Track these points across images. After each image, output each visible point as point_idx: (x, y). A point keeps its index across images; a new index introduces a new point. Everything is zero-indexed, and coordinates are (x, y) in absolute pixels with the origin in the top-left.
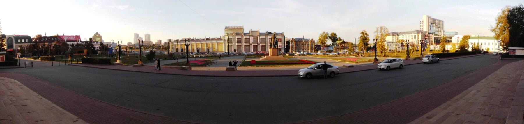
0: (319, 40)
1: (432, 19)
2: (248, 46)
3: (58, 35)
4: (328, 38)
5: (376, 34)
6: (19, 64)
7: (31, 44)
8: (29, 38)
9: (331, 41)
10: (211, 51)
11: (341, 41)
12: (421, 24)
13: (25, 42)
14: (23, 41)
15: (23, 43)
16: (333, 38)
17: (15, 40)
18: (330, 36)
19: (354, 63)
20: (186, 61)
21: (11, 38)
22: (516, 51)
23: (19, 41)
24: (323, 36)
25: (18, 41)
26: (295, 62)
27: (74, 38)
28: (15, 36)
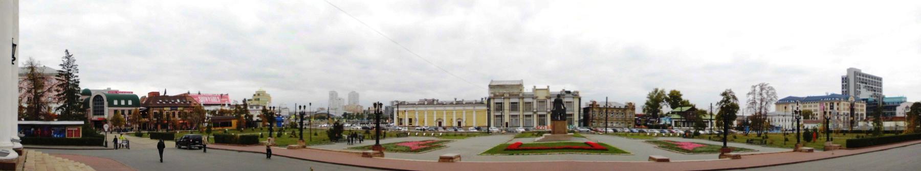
0: (646, 105)
1: (863, 75)
2: (530, 116)
3: (189, 93)
4: (664, 100)
5: (751, 97)
6: (106, 143)
7: (136, 110)
8: (134, 98)
9: (669, 106)
11: (690, 108)
12: (845, 84)
13: (126, 105)
14: (123, 103)
16: (673, 101)
17: (107, 101)
18: (668, 96)
21: (101, 97)
23: (116, 103)
24: (655, 96)
25: (113, 103)
26: (544, 147)
27: (218, 100)
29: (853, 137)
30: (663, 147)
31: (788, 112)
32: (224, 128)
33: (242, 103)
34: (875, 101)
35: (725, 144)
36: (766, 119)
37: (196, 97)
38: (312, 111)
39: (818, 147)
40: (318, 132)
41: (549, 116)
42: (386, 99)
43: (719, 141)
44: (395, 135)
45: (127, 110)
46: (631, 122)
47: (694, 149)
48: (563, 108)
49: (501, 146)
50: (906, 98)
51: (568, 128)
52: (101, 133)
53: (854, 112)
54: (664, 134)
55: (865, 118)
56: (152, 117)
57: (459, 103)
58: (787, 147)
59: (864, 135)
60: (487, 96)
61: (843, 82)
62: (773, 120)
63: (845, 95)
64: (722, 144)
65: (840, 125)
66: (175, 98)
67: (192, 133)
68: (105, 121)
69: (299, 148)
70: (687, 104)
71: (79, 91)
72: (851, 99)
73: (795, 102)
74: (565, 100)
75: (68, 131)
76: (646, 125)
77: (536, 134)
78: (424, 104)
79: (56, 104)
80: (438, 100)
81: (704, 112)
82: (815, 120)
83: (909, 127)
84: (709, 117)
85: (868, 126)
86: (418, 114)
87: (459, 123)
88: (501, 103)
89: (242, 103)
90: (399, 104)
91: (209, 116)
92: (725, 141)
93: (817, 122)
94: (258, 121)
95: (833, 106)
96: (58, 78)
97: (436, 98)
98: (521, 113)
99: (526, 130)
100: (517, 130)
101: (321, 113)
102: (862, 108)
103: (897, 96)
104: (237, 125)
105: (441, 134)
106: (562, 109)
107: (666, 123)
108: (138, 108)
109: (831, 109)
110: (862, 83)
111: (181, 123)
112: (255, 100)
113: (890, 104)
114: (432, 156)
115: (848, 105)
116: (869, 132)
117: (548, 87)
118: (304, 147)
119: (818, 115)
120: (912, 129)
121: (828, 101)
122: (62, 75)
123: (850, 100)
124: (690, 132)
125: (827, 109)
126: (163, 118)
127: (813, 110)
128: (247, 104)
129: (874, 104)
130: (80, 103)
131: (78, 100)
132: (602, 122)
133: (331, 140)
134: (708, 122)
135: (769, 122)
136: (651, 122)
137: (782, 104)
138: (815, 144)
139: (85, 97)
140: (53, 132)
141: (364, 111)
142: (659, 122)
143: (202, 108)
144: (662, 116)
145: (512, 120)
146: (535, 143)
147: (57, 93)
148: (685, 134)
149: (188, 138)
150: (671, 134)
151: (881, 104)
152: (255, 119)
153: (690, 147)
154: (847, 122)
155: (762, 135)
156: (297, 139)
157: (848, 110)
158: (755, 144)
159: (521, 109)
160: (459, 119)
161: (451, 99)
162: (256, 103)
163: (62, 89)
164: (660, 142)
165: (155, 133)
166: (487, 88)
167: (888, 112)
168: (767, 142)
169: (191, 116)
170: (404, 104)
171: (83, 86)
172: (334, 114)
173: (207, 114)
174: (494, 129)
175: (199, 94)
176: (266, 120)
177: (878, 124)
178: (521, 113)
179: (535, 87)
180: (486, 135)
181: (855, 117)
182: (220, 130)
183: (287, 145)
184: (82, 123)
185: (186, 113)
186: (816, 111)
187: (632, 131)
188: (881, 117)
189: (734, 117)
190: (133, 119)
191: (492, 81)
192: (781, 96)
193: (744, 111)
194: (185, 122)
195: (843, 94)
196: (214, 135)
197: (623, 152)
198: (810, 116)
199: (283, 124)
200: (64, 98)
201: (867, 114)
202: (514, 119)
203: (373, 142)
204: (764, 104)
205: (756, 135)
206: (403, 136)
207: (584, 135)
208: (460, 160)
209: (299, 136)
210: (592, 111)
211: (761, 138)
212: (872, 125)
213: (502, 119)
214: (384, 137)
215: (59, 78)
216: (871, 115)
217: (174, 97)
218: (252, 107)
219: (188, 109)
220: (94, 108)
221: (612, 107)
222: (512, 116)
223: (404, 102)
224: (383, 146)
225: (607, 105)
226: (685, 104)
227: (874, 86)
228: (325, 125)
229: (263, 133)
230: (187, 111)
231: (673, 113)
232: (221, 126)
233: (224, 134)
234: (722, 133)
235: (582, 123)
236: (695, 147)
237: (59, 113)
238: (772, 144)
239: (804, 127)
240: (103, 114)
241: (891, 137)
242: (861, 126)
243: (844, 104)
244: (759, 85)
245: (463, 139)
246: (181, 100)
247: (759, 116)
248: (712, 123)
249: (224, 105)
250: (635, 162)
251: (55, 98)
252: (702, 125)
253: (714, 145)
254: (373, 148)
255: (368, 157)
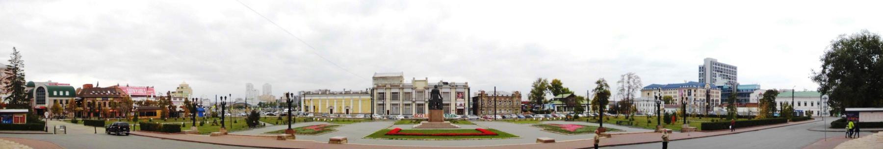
2: (409, 105)
4: (547, 88)
5: (620, 85)
6: (47, 128)
7: (72, 100)
8: (71, 90)
9: (552, 94)
10: (320, 111)
11: (569, 95)
12: (701, 72)
13: (64, 96)
14: (61, 93)
15: (61, 96)
17: (48, 92)
18: (550, 85)
19: (186, 131)
20: (292, 125)
21: (43, 88)
22: (860, 115)
23: (55, 93)
24: (539, 85)
25: (53, 94)
26: (421, 133)
28: (48, 85)
29: (708, 120)
30: (548, 130)
31: (651, 97)
32: (150, 117)
33: (167, 95)
34: (730, 88)
35: (601, 125)
36: (633, 103)
37: (125, 88)
38: (231, 101)
39: (676, 128)
40: (238, 120)
41: (427, 105)
42: (295, 89)
43: (595, 123)
44: (303, 120)
45: (65, 100)
46: (518, 108)
47: (575, 130)
48: (439, 98)
49: (382, 131)
50: (759, 86)
51: (445, 117)
52: (42, 120)
53: (710, 98)
54: (548, 118)
55: (720, 104)
56: (86, 106)
57: (347, 93)
58: (650, 129)
59: (719, 119)
60: (371, 87)
61: (700, 71)
62: (639, 104)
63: (702, 83)
64: (598, 125)
65: (696, 109)
66: (106, 89)
67: (120, 121)
68: (46, 109)
69: (221, 135)
70: (567, 91)
71: (24, 83)
72: (708, 86)
73: (658, 89)
74: (441, 91)
75: (15, 117)
76: (531, 111)
77: (414, 121)
78: (318, 94)
79: (5, 94)
80: (329, 91)
81: (582, 99)
82: (675, 105)
83: (761, 112)
84: (586, 102)
85: (722, 111)
86: (329, 103)
87: (347, 111)
88: (383, 93)
89: (167, 95)
90: (306, 94)
91: (136, 106)
92: (600, 122)
93: (676, 107)
94: (180, 111)
95: (690, 93)
96: (7, 72)
97: (328, 89)
98: (401, 102)
99: (405, 117)
100: (397, 117)
101: (239, 103)
102: (717, 95)
103: (751, 84)
104: (161, 114)
105: (332, 119)
106: (439, 99)
107: (550, 109)
108: (74, 98)
109: (688, 95)
110: (718, 71)
111: (111, 112)
112: (179, 92)
113: (744, 91)
114: (324, 138)
115: (704, 91)
116: (722, 116)
117: (427, 78)
118: (226, 134)
119: (678, 101)
120: (764, 115)
121: (686, 88)
122: (10, 69)
123: (706, 87)
124: (571, 116)
125: (685, 95)
126: (95, 107)
127: (673, 97)
128: (171, 96)
129: (729, 91)
130: (25, 93)
131: (23, 91)
132: (490, 110)
133: (250, 127)
134: (585, 107)
135: (635, 106)
136: (536, 108)
137: (646, 90)
138: (673, 126)
139: (29, 89)
140: (2, 118)
141: (277, 100)
142: (543, 108)
143: (130, 99)
144: (546, 102)
145: (393, 108)
146: (413, 129)
147: (5, 85)
148: (567, 118)
149: (116, 125)
150: (555, 118)
151: (735, 91)
152: (178, 109)
153: (571, 129)
154: (703, 107)
155: (629, 118)
156: (219, 127)
157: (704, 96)
158: (623, 125)
159: (401, 99)
160: (347, 107)
161: (341, 90)
162: (179, 95)
163: (10, 82)
164: (545, 126)
165: (88, 120)
166: (372, 79)
167: (742, 98)
168: (633, 124)
169: (120, 106)
170: (310, 94)
171: (27, 80)
172: (251, 104)
173: (134, 105)
174: (376, 116)
175: (128, 86)
176: (189, 110)
177: (732, 110)
178: (401, 102)
179: (414, 78)
180: (370, 121)
181: (711, 102)
182: (145, 119)
183: (210, 133)
184: (27, 110)
185: (115, 103)
186: (676, 97)
187: (519, 117)
188: (735, 103)
189: (607, 102)
190: (69, 108)
191: (376, 74)
192: (646, 83)
193: (615, 97)
194: (115, 111)
195: (700, 82)
196: (140, 123)
197: (512, 136)
198: (670, 102)
199: (204, 113)
200: (12, 90)
201: (722, 100)
202: (394, 108)
203: (286, 127)
204: (631, 90)
205: (625, 118)
206: (310, 121)
207: (474, 122)
208: (347, 142)
209: (221, 125)
210: (482, 100)
211: (628, 120)
212: (726, 110)
213: (383, 108)
214: (294, 122)
215: (8, 72)
216: (726, 101)
217: (106, 88)
218: (175, 99)
219: (118, 99)
220: (37, 97)
221: (499, 96)
222: (393, 104)
223: (309, 92)
224: (294, 130)
225: (495, 94)
226: (565, 91)
227: (729, 75)
228: (243, 113)
229: (186, 123)
230: (116, 101)
231: (555, 99)
232: (147, 115)
233: (149, 122)
234: (597, 116)
235: (472, 112)
236: (575, 128)
237: (7, 102)
238: (637, 126)
239: (665, 111)
240: (45, 104)
241: (744, 121)
242: (716, 112)
243: (701, 91)
244: (627, 74)
245: (350, 124)
246: (111, 92)
247: (626, 101)
248: (588, 107)
249: (150, 96)
250: (524, 144)
251: (4, 90)
252: (581, 110)
253: (591, 126)
254: (287, 131)
255: (282, 139)
